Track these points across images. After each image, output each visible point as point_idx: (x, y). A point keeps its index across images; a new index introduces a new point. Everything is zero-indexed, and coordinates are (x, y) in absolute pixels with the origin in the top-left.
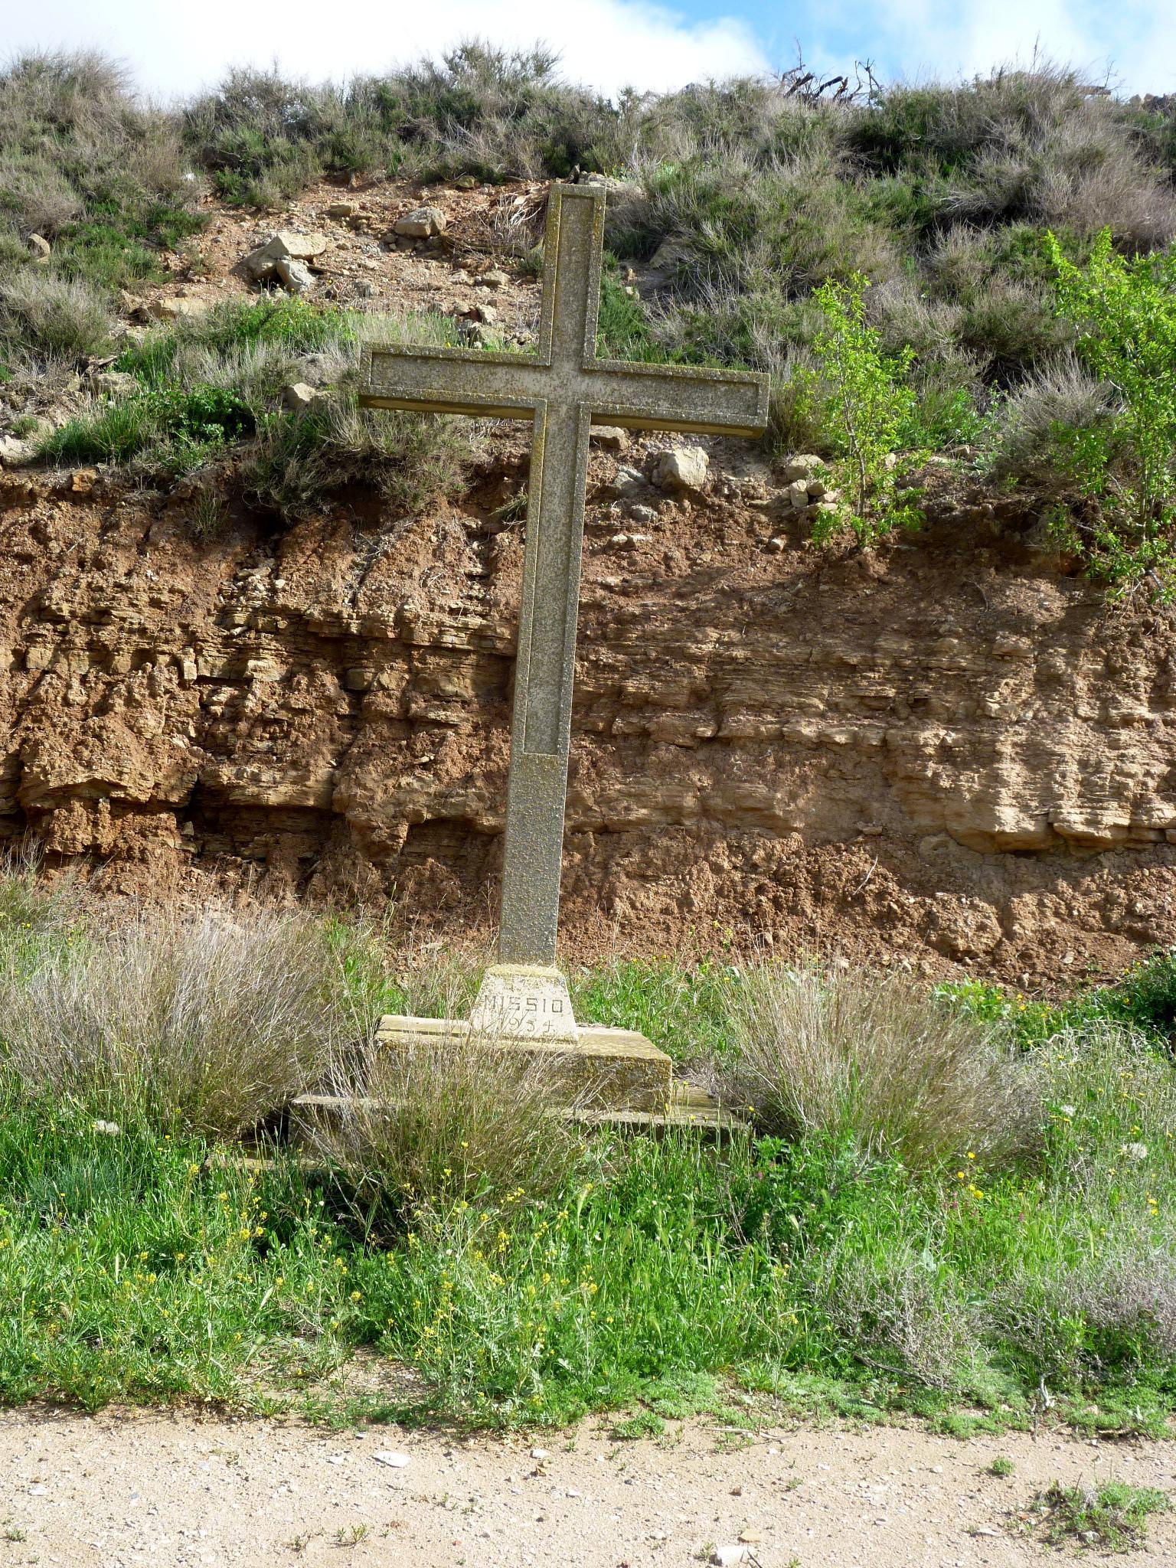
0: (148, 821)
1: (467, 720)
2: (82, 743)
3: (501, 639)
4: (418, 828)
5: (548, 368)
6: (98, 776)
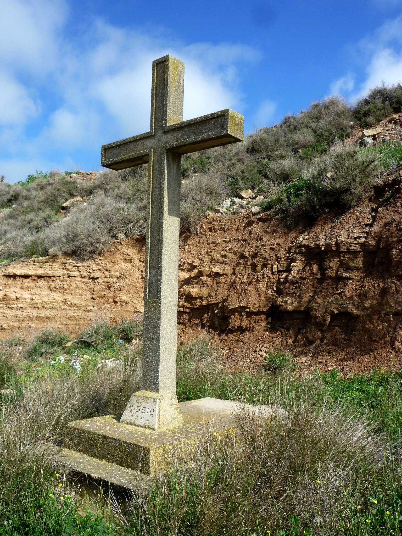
0: (257, 318)
1: (358, 276)
2: (241, 295)
3: (372, 245)
4: (333, 316)
5: (154, 136)
6: (241, 305)
